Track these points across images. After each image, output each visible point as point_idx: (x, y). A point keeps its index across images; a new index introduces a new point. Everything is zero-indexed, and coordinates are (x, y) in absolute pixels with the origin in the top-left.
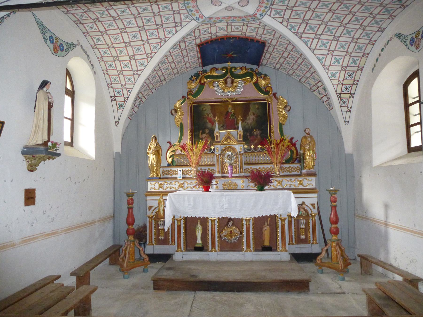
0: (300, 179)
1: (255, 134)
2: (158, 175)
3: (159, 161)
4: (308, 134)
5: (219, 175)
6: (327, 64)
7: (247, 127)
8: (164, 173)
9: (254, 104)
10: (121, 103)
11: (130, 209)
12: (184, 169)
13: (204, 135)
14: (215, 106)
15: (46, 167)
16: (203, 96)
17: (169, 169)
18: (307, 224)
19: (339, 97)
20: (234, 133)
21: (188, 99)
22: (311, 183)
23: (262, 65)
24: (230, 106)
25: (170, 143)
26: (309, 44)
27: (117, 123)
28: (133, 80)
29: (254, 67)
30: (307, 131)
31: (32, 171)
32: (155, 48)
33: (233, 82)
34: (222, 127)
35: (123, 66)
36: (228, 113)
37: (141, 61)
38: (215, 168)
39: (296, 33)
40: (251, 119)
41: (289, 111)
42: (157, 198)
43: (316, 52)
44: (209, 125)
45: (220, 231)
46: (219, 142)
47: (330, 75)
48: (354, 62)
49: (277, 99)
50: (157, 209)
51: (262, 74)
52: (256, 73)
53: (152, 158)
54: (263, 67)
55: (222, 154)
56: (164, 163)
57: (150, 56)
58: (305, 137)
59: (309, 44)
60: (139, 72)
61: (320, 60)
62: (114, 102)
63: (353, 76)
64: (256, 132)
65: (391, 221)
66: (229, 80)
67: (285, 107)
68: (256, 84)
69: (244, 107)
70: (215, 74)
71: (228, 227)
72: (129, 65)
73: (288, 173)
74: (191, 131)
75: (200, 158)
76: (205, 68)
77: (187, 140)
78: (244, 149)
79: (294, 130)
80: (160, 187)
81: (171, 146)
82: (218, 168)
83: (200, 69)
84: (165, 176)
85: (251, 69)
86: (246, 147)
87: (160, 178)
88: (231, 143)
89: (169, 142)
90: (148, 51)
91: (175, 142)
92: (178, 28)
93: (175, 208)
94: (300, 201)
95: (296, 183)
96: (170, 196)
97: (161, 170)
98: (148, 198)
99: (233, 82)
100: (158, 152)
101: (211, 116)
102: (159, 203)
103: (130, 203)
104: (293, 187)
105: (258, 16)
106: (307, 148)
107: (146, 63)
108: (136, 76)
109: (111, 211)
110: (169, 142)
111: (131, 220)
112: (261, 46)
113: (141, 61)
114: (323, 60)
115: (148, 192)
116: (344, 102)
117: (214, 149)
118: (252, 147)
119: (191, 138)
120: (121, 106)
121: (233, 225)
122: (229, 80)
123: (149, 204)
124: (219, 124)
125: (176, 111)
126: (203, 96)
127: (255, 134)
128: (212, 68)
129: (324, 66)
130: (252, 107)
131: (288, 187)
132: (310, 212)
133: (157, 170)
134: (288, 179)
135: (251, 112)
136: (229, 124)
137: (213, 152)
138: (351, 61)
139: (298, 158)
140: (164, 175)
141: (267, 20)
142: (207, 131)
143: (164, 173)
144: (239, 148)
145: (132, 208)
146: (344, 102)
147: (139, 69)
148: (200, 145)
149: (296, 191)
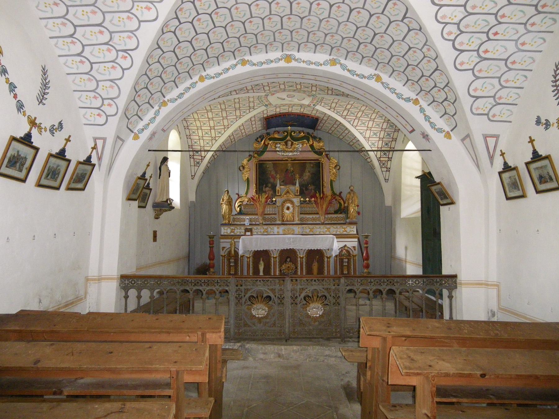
0: (344, 226)
1: (310, 188)
2: (229, 222)
3: (231, 210)
4: (352, 190)
5: (280, 222)
6: (367, 136)
7: (303, 182)
8: (234, 220)
9: (310, 163)
10: (198, 160)
11: (211, 248)
12: (251, 217)
13: (267, 189)
14: (276, 163)
15: (165, 215)
16: (267, 156)
17: (238, 217)
18: (349, 262)
19: (379, 160)
20: (292, 187)
21: (254, 157)
22: (352, 230)
23: (317, 130)
24: (289, 165)
25: (238, 195)
26: (352, 122)
27: (193, 177)
28: (211, 143)
29: (311, 131)
30: (352, 188)
31: (157, 218)
32: (232, 121)
33: (292, 144)
34: (283, 182)
35: (204, 133)
36: (287, 170)
37: (219, 130)
38: (276, 216)
39: (342, 116)
40: (307, 175)
41: (339, 169)
42: (230, 240)
43: (357, 128)
44: (272, 180)
45: (280, 266)
46: (280, 196)
47: (370, 144)
48: (388, 135)
49: (329, 159)
50: (229, 250)
51: (317, 138)
52: (312, 137)
53: (225, 207)
54: (319, 131)
55: (283, 206)
56: (234, 212)
57: (226, 127)
58: (349, 193)
59: (352, 122)
60: (217, 138)
61: (361, 133)
62: (192, 160)
63: (389, 144)
64: (311, 187)
65: (408, 259)
66: (290, 143)
67: (336, 166)
68: (312, 146)
69: (302, 164)
70: (276, 136)
71: (286, 263)
72: (209, 133)
73: (336, 222)
74: (256, 185)
75: (264, 208)
76: (268, 131)
77: (253, 192)
78: (301, 201)
79: (342, 186)
80: (231, 232)
81: (239, 197)
82: (279, 217)
83: (264, 131)
84: (236, 223)
85: (308, 133)
86: (302, 199)
87: (231, 224)
88: (290, 201)
89: (237, 194)
90: (226, 124)
91: (242, 192)
92: (251, 110)
93: (244, 247)
94: (342, 245)
95: (340, 230)
96: (243, 239)
97: (232, 217)
98: (222, 240)
99: (292, 144)
100: (230, 203)
101: (273, 173)
102: (231, 245)
103: (211, 243)
104: (338, 233)
105: (312, 105)
106: (351, 201)
107: (223, 132)
108: (214, 141)
109: (186, 250)
110: (237, 194)
111: (212, 257)
112: (317, 119)
113: (219, 130)
114: (364, 134)
115: (222, 235)
116: (384, 164)
117: (275, 201)
118: (307, 199)
119: (256, 191)
120: (198, 163)
121: (290, 261)
122: (290, 143)
123: (222, 245)
124: (280, 180)
125: (244, 168)
126: (267, 156)
127: (310, 188)
128: (275, 131)
129: (365, 137)
130: (308, 165)
131: (334, 233)
132: (351, 252)
133: (229, 217)
134: (335, 226)
135: (307, 170)
136: (288, 181)
137: (274, 204)
138: (386, 134)
139: (343, 210)
140: (234, 222)
141: (318, 107)
142: (270, 185)
143: (234, 220)
144: (296, 201)
145: (213, 247)
146: (384, 164)
147: (217, 135)
148: (264, 196)
149: (339, 236)
